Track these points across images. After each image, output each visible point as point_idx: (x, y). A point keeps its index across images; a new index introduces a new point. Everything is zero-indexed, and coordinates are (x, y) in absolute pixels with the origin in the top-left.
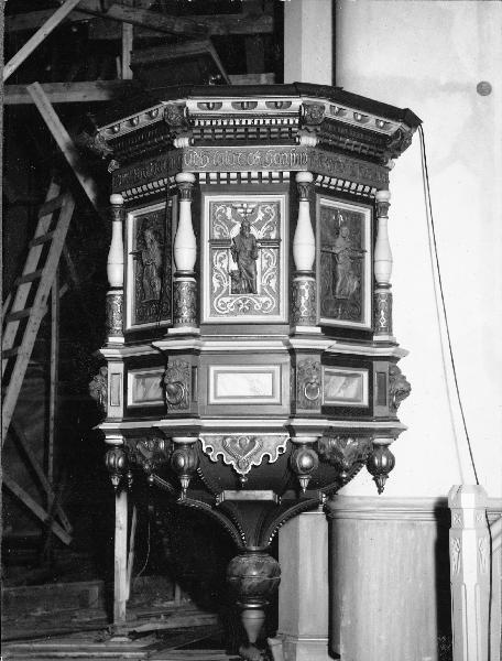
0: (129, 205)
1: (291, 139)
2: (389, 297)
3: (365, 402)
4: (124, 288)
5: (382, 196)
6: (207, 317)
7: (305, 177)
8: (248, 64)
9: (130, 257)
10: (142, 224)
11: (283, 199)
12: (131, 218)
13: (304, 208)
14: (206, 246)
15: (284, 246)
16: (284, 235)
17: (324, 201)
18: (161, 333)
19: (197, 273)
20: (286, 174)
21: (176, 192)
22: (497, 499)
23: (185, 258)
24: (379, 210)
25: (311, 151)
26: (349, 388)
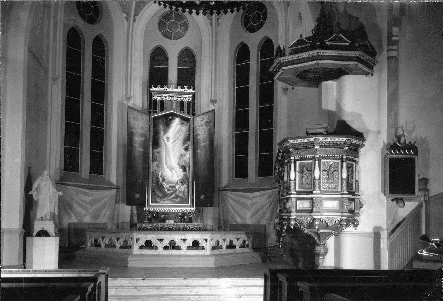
0: (296, 160)
1: (342, 147)
2: (358, 183)
3: (298, 201)
4: (295, 180)
5: (357, 159)
6: (322, 189)
7: (344, 156)
8: (143, 59)
9: (297, 172)
10: (302, 166)
11: (339, 161)
12: (297, 162)
13: (344, 163)
14: (321, 172)
15: (339, 172)
16: (339, 169)
17: (348, 162)
18: (311, 192)
19: (319, 178)
20: (341, 156)
21: (314, 158)
22: (132, 208)
23: (317, 175)
24: (357, 162)
25: (347, 150)
26: (353, 205)
